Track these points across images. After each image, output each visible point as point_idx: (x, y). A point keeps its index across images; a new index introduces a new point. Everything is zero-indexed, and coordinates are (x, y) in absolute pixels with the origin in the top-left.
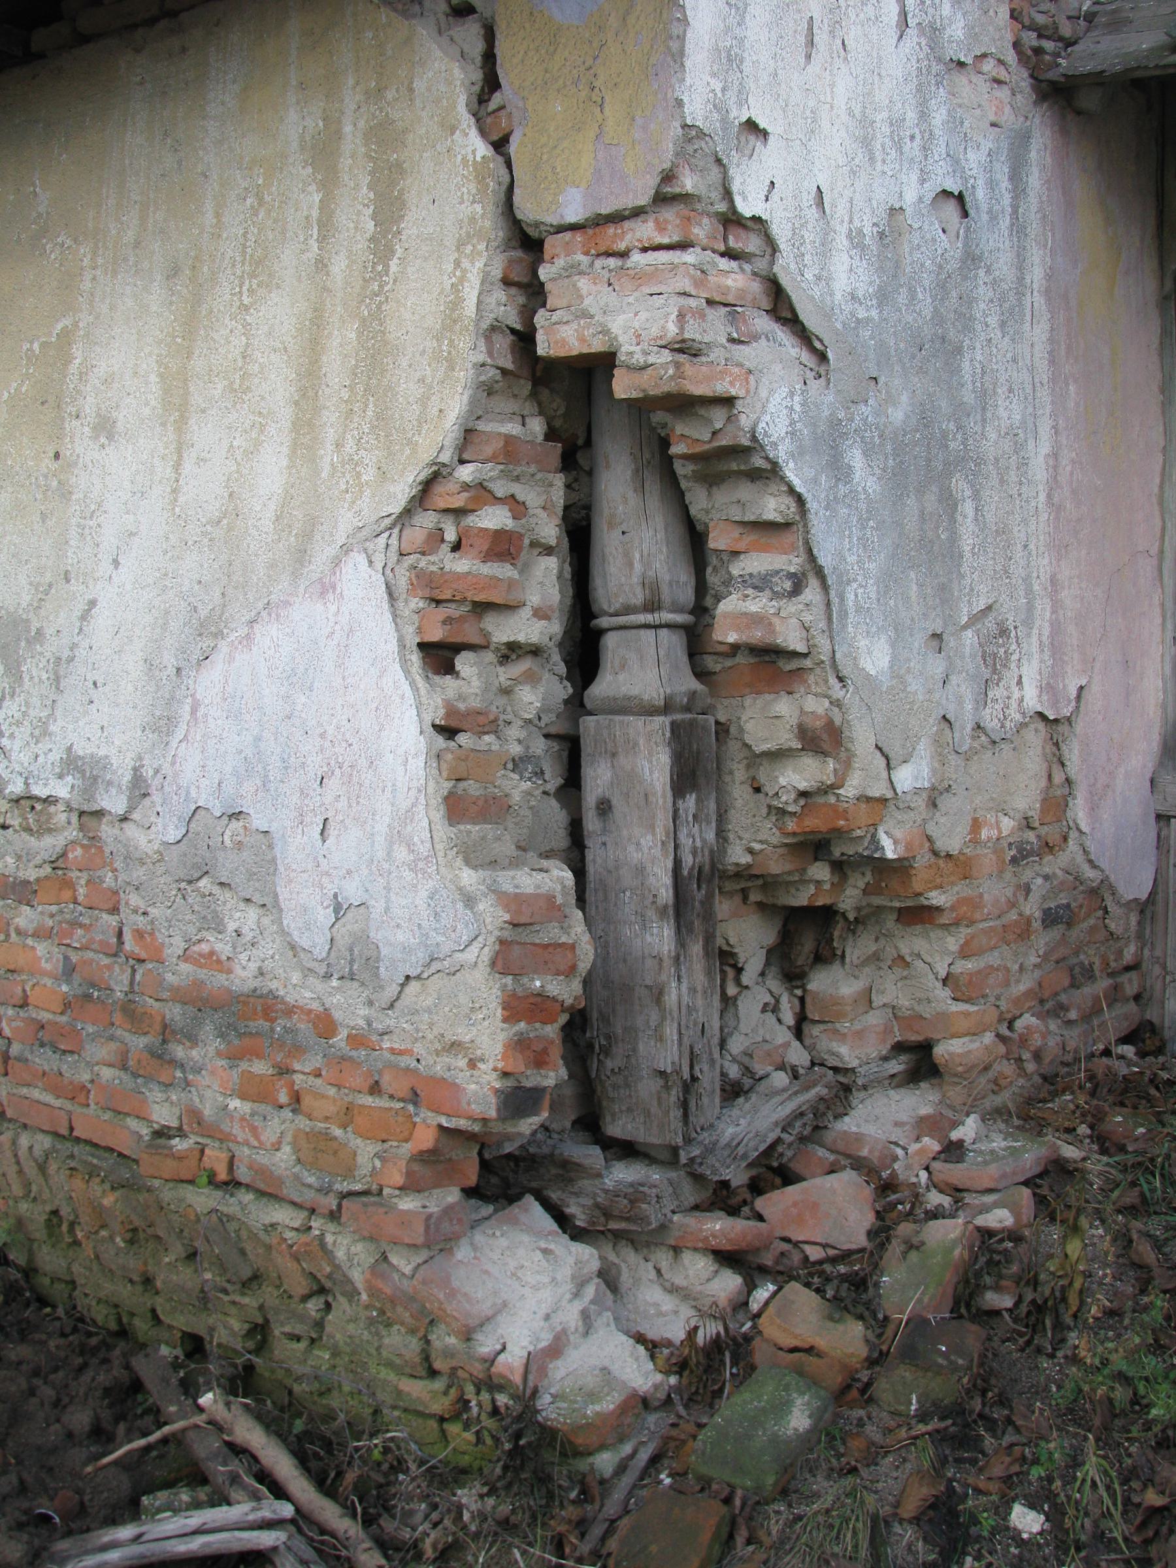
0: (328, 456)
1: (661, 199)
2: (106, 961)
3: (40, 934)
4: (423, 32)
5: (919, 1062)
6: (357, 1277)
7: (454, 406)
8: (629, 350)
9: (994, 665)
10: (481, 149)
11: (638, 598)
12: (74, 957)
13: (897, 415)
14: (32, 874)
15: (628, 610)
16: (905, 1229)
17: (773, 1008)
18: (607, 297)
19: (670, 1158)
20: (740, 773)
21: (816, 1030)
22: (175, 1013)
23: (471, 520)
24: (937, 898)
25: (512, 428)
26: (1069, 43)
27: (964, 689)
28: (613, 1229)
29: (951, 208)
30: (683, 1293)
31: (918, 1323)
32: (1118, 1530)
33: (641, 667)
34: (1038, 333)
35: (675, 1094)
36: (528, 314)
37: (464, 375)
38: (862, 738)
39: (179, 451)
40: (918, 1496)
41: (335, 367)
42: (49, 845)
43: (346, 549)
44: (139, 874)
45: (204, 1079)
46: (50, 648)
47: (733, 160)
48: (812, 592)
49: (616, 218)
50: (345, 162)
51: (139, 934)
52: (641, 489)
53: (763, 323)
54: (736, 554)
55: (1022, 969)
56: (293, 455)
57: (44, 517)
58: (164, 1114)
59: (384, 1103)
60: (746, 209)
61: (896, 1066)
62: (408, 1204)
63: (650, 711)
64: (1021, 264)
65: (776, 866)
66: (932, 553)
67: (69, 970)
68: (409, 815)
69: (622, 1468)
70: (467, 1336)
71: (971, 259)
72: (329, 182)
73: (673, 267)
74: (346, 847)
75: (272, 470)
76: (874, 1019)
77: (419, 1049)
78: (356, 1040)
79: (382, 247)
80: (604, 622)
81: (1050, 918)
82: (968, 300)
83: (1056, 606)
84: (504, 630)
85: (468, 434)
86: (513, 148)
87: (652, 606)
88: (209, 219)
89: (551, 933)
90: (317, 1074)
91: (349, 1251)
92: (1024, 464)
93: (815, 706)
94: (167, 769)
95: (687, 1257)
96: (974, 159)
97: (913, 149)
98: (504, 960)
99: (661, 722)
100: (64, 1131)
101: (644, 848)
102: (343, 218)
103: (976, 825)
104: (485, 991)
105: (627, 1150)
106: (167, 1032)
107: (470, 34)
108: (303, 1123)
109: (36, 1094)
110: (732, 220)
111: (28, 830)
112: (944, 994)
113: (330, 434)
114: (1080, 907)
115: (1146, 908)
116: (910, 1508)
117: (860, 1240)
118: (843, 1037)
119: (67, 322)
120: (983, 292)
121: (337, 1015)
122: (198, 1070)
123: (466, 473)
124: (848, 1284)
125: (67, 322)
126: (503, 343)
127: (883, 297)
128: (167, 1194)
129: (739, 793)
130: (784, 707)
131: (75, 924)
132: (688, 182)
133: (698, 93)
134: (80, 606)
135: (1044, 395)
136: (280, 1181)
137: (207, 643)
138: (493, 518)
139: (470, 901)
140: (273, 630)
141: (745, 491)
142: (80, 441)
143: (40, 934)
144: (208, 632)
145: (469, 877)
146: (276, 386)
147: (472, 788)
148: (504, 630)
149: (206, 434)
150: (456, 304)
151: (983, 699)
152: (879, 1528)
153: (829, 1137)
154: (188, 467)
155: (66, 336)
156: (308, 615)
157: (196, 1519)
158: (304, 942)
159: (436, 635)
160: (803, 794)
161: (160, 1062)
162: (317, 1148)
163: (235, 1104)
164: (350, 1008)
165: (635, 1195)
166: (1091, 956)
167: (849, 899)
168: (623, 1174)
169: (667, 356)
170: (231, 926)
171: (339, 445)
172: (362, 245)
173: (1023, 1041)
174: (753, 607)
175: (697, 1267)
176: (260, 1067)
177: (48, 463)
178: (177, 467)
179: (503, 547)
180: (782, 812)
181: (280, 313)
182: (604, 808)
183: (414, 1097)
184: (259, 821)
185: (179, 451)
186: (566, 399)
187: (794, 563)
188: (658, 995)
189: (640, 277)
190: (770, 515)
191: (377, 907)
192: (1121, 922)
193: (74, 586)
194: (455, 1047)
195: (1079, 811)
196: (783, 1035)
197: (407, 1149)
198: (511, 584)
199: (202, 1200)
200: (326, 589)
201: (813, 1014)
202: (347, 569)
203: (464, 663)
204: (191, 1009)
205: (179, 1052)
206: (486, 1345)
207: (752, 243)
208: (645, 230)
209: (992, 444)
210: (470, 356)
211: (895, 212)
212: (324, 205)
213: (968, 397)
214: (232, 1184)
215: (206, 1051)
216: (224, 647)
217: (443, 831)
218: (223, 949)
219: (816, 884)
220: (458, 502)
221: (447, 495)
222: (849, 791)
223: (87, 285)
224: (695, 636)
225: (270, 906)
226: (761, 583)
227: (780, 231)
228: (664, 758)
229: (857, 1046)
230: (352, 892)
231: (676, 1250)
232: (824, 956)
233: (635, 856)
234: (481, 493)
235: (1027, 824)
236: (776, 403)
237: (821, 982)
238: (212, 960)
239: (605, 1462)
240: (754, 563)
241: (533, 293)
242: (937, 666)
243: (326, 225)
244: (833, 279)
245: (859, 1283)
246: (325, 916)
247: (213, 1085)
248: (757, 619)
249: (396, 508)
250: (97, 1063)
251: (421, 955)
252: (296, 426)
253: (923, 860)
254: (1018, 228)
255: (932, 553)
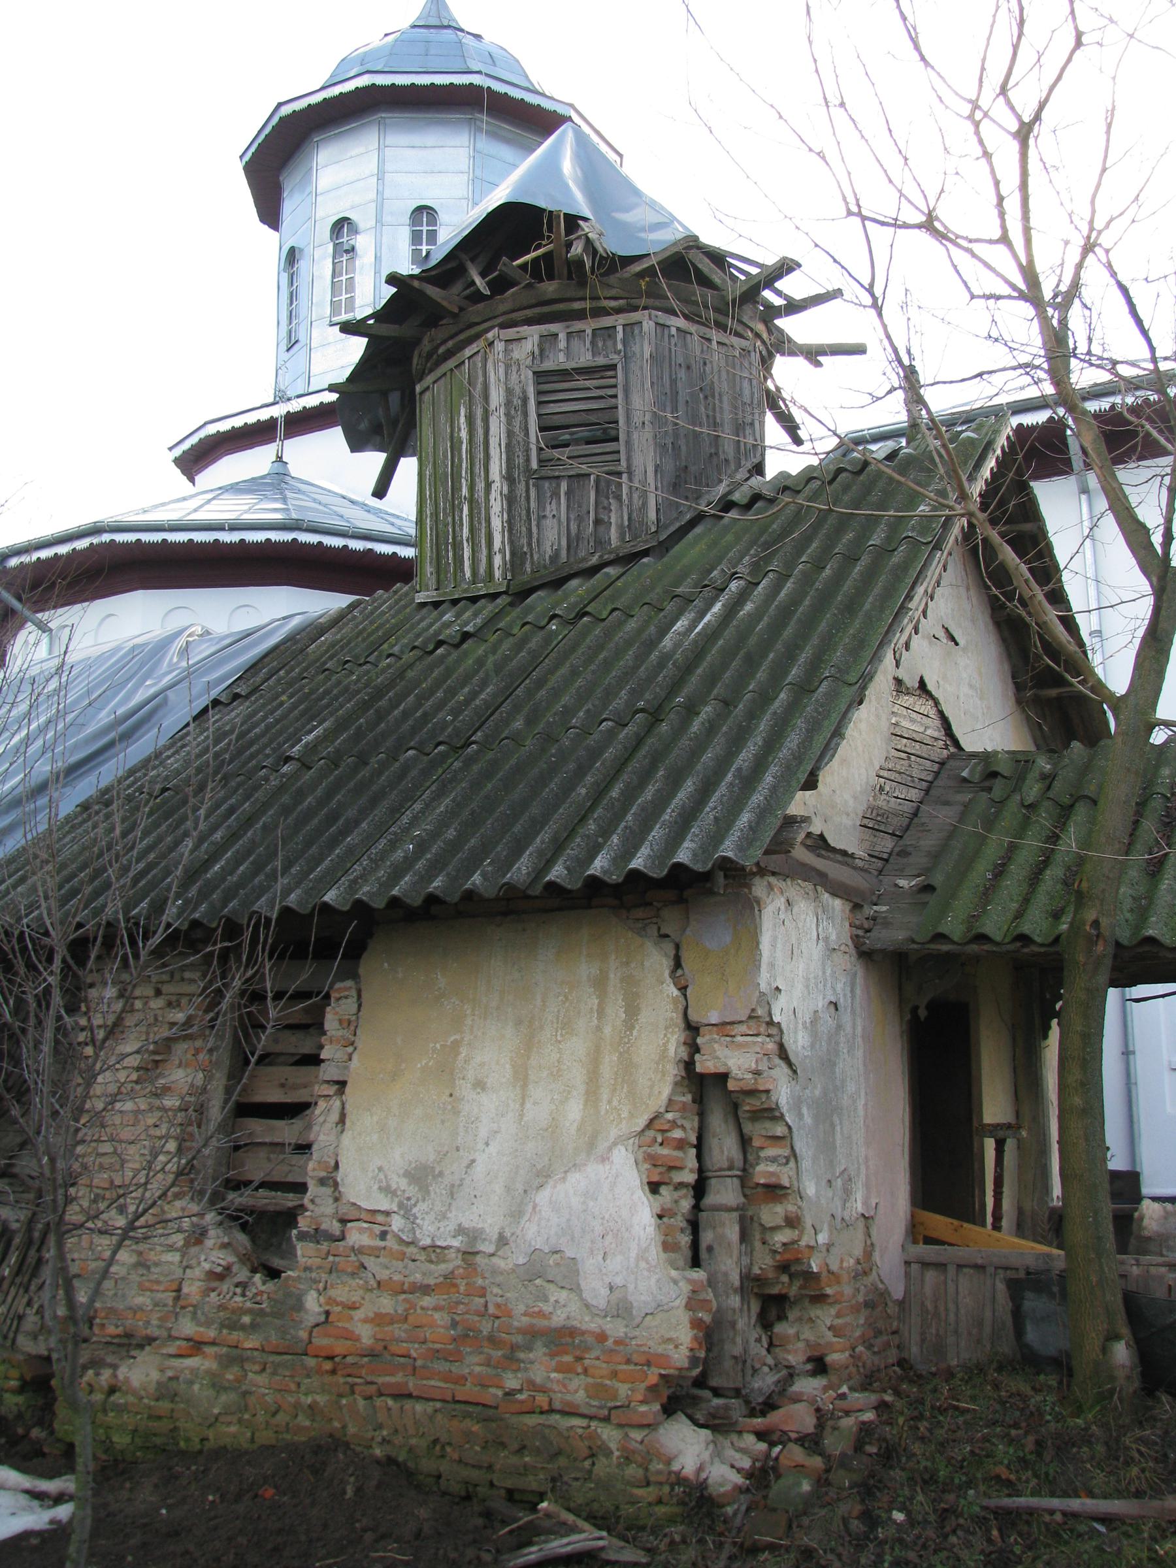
0: (604, 1107)
1: (750, 1017)
2: (476, 1318)
3: (437, 1308)
4: (649, 945)
5: (819, 1366)
6: (613, 1446)
7: (666, 1090)
8: (735, 1072)
9: (847, 1192)
10: (676, 992)
11: (726, 1165)
12: (458, 1318)
13: (817, 1093)
14: (432, 1282)
15: (721, 1170)
16: (830, 1423)
17: (759, 1340)
18: (727, 1052)
19: (737, 1393)
20: (758, 1236)
21: (777, 1350)
22: (519, 1339)
23: (669, 1134)
24: (829, 1291)
25: (683, 1099)
26: (868, 931)
27: (838, 1203)
28: (718, 1425)
29: (832, 1008)
30: (746, 1449)
31: (843, 1455)
32: (932, 1518)
33: (725, 1193)
34: (859, 1054)
35: (740, 1366)
36: (692, 1056)
37: (670, 1079)
38: (808, 1221)
39: (523, 1098)
40: (858, 1508)
41: (607, 1070)
42: (443, 1268)
43: (615, 1144)
44: (499, 1279)
45: (536, 1366)
46: (447, 1180)
47: (772, 1002)
48: (792, 1164)
49: (733, 1023)
50: (610, 989)
51: (498, 1306)
52: (726, 1122)
53: (777, 1061)
54: (762, 1148)
55: (857, 1324)
56: (585, 1105)
57: (443, 1122)
58: (512, 1382)
59: (632, 1367)
60: (776, 1019)
61: (809, 1367)
62: (643, 1408)
63: (729, 1209)
64: (854, 1027)
65: (771, 1275)
66: (827, 1147)
67: (454, 1324)
68: (647, 1249)
69: (735, 1513)
70: (668, 1462)
71: (839, 1027)
72: (602, 994)
73: (755, 1043)
74: (616, 1263)
75: (574, 1111)
76: (801, 1345)
77: (650, 1343)
78: (617, 1342)
79: (629, 1025)
80: (710, 1174)
81: (867, 1304)
82: (837, 1043)
83: (867, 1168)
84: (678, 1177)
85: (670, 1101)
86: (689, 991)
87: (730, 1168)
88: (539, 1002)
89: (702, 1296)
90: (598, 1358)
91: (609, 1435)
92: (856, 1109)
93: (791, 1208)
94: (518, 1232)
95: (745, 1435)
96: (839, 986)
97: (821, 986)
98: (689, 1306)
99: (735, 1215)
100: (449, 1398)
101: (729, 1265)
102: (610, 1010)
103: (842, 1261)
104: (684, 1317)
105: (717, 1393)
106: (514, 1348)
107: (669, 948)
108: (590, 1380)
109: (432, 1383)
110: (770, 1023)
111: (431, 1262)
112: (830, 1334)
113: (605, 1097)
114: (876, 1301)
115: (901, 1303)
116: (855, 1513)
117: (811, 1430)
118: (789, 1352)
119: (457, 1037)
120: (842, 1039)
121: (609, 1333)
122: (532, 1362)
123: (670, 1116)
124: (812, 1442)
125: (457, 1037)
126: (682, 1066)
127: (812, 1046)
128: (514, 1420)
129: (757, 1244)
130: (779, 1209)
131: (458, 1303)
132: (760, 1012)
133: (764, 980)
134: (465, 1162)
135: (862, 1079)
136: (578, 1406)
137: (540, 1180)
138: (677, 1134)
139: (675, 1282)
140: (577, 1175)
141: (768, 1124)
142: (465, 1089)
143: (437, 1308)
144: (542, 1176)
145: (674, 1273)
146: (577, 1076)
147: (669, 1239)
148: (678, 1177)
149: (537, 1092)
150: (666, 1050)
151: (844, 1208)
152: (845, 1521)
153: (788, 1393)
154: (528, 1105)
155: (456, 1044)
156: (594, 1170)
157: (565, 1540)
158: (594, 1303)
159: (656, 1178)
160: (784, 1244)
161: (511, 1359)
162: (596, 1391)
163: (553, 1375)
164: (616, 1329)
165: (727, 1408)
166: (880, 1324)
167: (793, 1291)
168: (717, 1401)
169: (750, 1076)
170: (552, 1299)
171: (610, 1102)
172: (619, 1023)
173: (859, 1358)
174: (771, 1169)
175: (750, 1439)
176: (568, 1358)
177: (445, 1098)
178: (523, 1104)
179: (681, 1145)
180: (775, 1252)
181: (577, 1047)
182: (710, 1249)
183: (648, 1364)
184: (569, 1253)
185: (523, 1098)
186: (702, 1087)
187: (786, 1152)
188: (733, 1324)
189: (740, 1046)
190: (779, 1134)
191: (631, 1287)
192: (892, 1310)
193: (461, 1153)
194: (670, 1340)
195: (876, 1256)
196: (764, 1352)
197: (643, 1385)
198: (682, 1159)
199: (532, 1420)
200: (604, 1159)
201: (776, 1342)
202: (615, 1152)
203: (663, 1190)
204: (528, 1337)
205: (522, 1355)
206: (675, 1467)
207: (773, 1031)
208: (743, 1028)
209: (845, 1101)
210: (673, 1071)
211: (816, 1012)
212: (599, 1004)
213: (838, 1083)
214: (552, 1411)
215: (539, 1352)
216: (551, 1182)
217: (663, 1256)
218: (547, 1308)
219: (783, 1285)
220: (666, 1127)
221: (658, 1124)
222: (803, 1243)
223: (469, 1022)
224: (745, 1178)
225: (576, 1289)
226: (773, 1160)
227: (784, 1026)
228: (737, 1228)
229: (795, 1357)
230: (619, 1281)
231: (740, 1433)
232: (782, 1317)
233: (723, 1268)
234: (674, 1124)
235: (858, 1262)
236: (783, 1093)
237: (779, 1328)
238: (541, 1314)
239: (729, 1510)
240: (770, 1152)
241: (694, 1049)
242: (830, 1193)
243: (601, 1013)
244: (798, 1042)
245: (817, 1443)
246: (604, 1292)
247: (540, 1367)
248: (772, 1174)
249: (639, 1129)
250: (473, 1364)
251: (654, 1305)
252: (587, 1093)
253: (824, 1274)
254: (853, 1012)
255: (827, 1147)
